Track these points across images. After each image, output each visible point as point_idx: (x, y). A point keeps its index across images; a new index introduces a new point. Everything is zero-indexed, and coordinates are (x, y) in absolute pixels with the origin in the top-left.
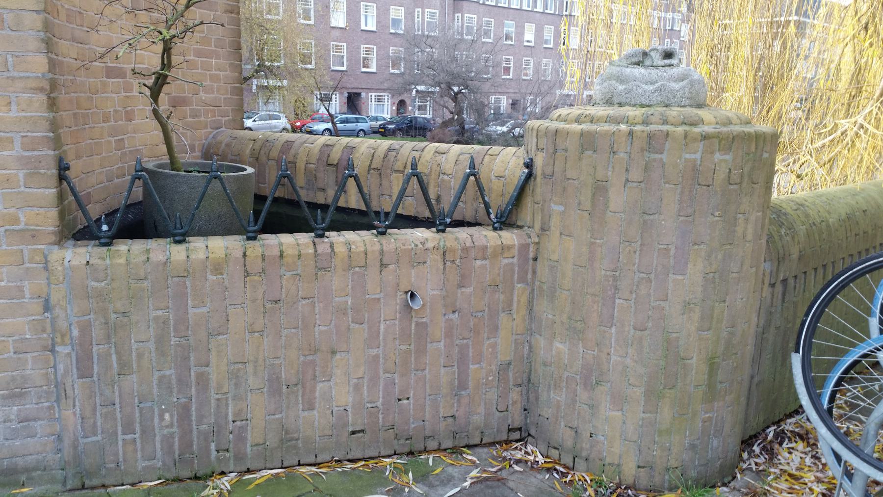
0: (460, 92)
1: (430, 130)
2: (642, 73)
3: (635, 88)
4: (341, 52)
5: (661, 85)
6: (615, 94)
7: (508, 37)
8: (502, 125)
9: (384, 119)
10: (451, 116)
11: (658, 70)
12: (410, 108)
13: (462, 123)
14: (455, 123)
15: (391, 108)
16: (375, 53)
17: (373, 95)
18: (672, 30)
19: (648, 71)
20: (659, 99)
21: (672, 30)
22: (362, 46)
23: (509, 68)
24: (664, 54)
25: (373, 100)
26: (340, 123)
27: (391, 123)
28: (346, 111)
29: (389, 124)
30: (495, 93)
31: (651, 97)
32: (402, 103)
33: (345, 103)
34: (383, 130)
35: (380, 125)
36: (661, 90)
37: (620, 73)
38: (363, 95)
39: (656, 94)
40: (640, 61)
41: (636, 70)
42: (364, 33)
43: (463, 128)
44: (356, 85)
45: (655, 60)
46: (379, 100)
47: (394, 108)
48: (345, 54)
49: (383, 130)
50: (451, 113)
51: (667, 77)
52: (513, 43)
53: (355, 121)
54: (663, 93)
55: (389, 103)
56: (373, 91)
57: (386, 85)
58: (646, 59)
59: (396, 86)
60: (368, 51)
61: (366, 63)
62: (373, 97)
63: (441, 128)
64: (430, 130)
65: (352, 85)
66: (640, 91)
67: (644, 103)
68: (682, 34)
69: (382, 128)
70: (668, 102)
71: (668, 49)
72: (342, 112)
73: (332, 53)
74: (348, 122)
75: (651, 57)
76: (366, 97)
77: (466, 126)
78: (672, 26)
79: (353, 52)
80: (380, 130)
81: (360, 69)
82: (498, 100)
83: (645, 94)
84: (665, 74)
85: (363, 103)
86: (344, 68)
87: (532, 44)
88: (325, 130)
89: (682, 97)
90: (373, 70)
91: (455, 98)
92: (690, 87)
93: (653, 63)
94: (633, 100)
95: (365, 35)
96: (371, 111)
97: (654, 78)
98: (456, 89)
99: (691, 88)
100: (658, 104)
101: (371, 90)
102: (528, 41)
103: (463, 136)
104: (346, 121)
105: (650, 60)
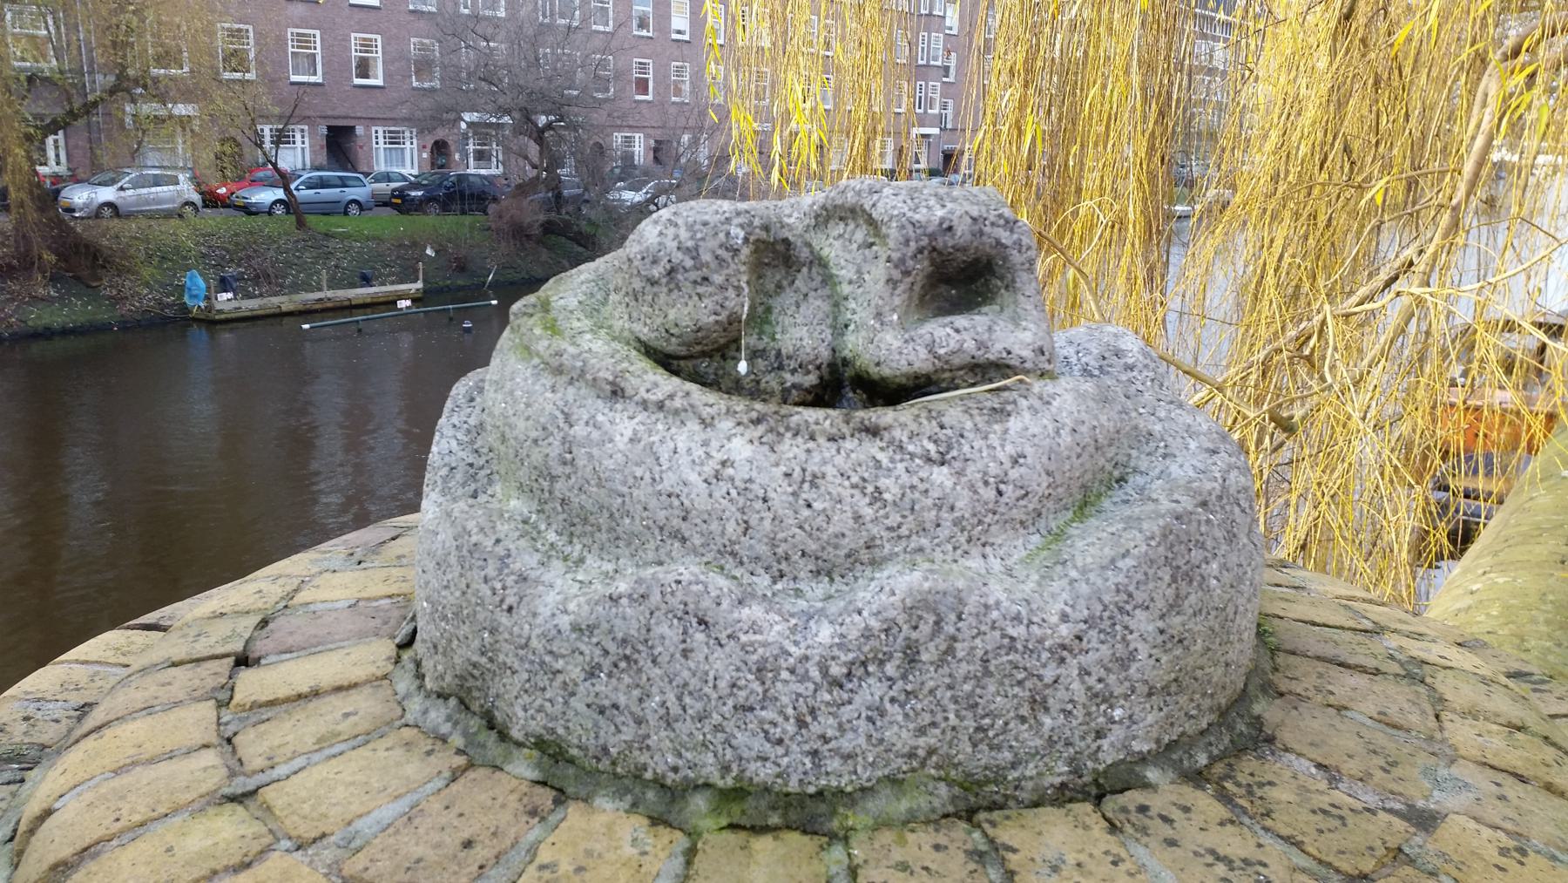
0: (549, 126)
1: (495, 199)
2: (741, 473)
3: (668, 631)
4: (310, 48)
5: (918, 607)
6: (507, 656)
7: (643, 24)
8: (637, 190)
9: (404, 178)
10: (532, 173)
11: (872, 448)
12: (457, 156)
13: (555, 186)
14: (542, 187)
15: (420, 156)
16: (380, 49)
17: (380, 130)
18: (930, 15)
19: (792, 449)
20: (900, 735)
21: (930, 15)
22: (353, 35)
23: (647, 80)
24: (922, 266)
25: (381, 140)
26: (308, 188)
27: (415, 186)
28: (325, 163)
29: (410, 189)
30: (620, 128)
31: (827, 724)
32: (440, 148)
33: (322, 147)
34: (399, 201)
35: (394, 190)
36: (911, 655)
37: (555, 448)
38: (360, 130)
39: (872, 690)
40: (733, 320)
41: (686, 437)
42: (356, 9)
43: (558, 196)
44: (340, 111)
45: (858, 312)
46: (394, 139)
47: (425, 155)
48: (319, 50)
49: (399, 201)
50: (534, 167)
51: (963, 502)
52: (650, 34)
53: (339, 182)
54: (932, 678)
55: (415, 145)
56: (378, 122)
57: (404, 111)
58: (788, 298)
59: (418, 114)
60: (367, 46)
61: (364, 69)
62: (381, 134)
63: (514, 197)
64: (495, 199)
65: (341, 111)
66: (722, 664)
67: (763, 773)
68: (948, 23)
69: (396, 197)
70: (985, 756)
71: (962, 229)
72: (317, 164)
73: (290, 50)
74: (323, 187)
75: (828, 280)
76: (366, 135)
77: (566, 192)
78: (931, 8)
79: (336, 47)
80: (394, 200)
81: (351, 79)
82: (629, 141)
83: (767, 699)
84: (941, 475)
85: (361, 147)
86: (318, 79)
87: (686, 37)
88: (275, 202)
89: (1108, 699)
90: (379, 82)
91: (539, 135)
92: (1163, 592)
93: (840, 329)
94: (659, 738)
95: (359, 15)
96: (378, 164)
97: (841, 521)
98: (542, 120)
99: (1175, 606)
100: (894, 781)
101: (374, 120)
102: (679, 32)
103: (559, 213)
104: (323, 184)
105: (817, 305)
